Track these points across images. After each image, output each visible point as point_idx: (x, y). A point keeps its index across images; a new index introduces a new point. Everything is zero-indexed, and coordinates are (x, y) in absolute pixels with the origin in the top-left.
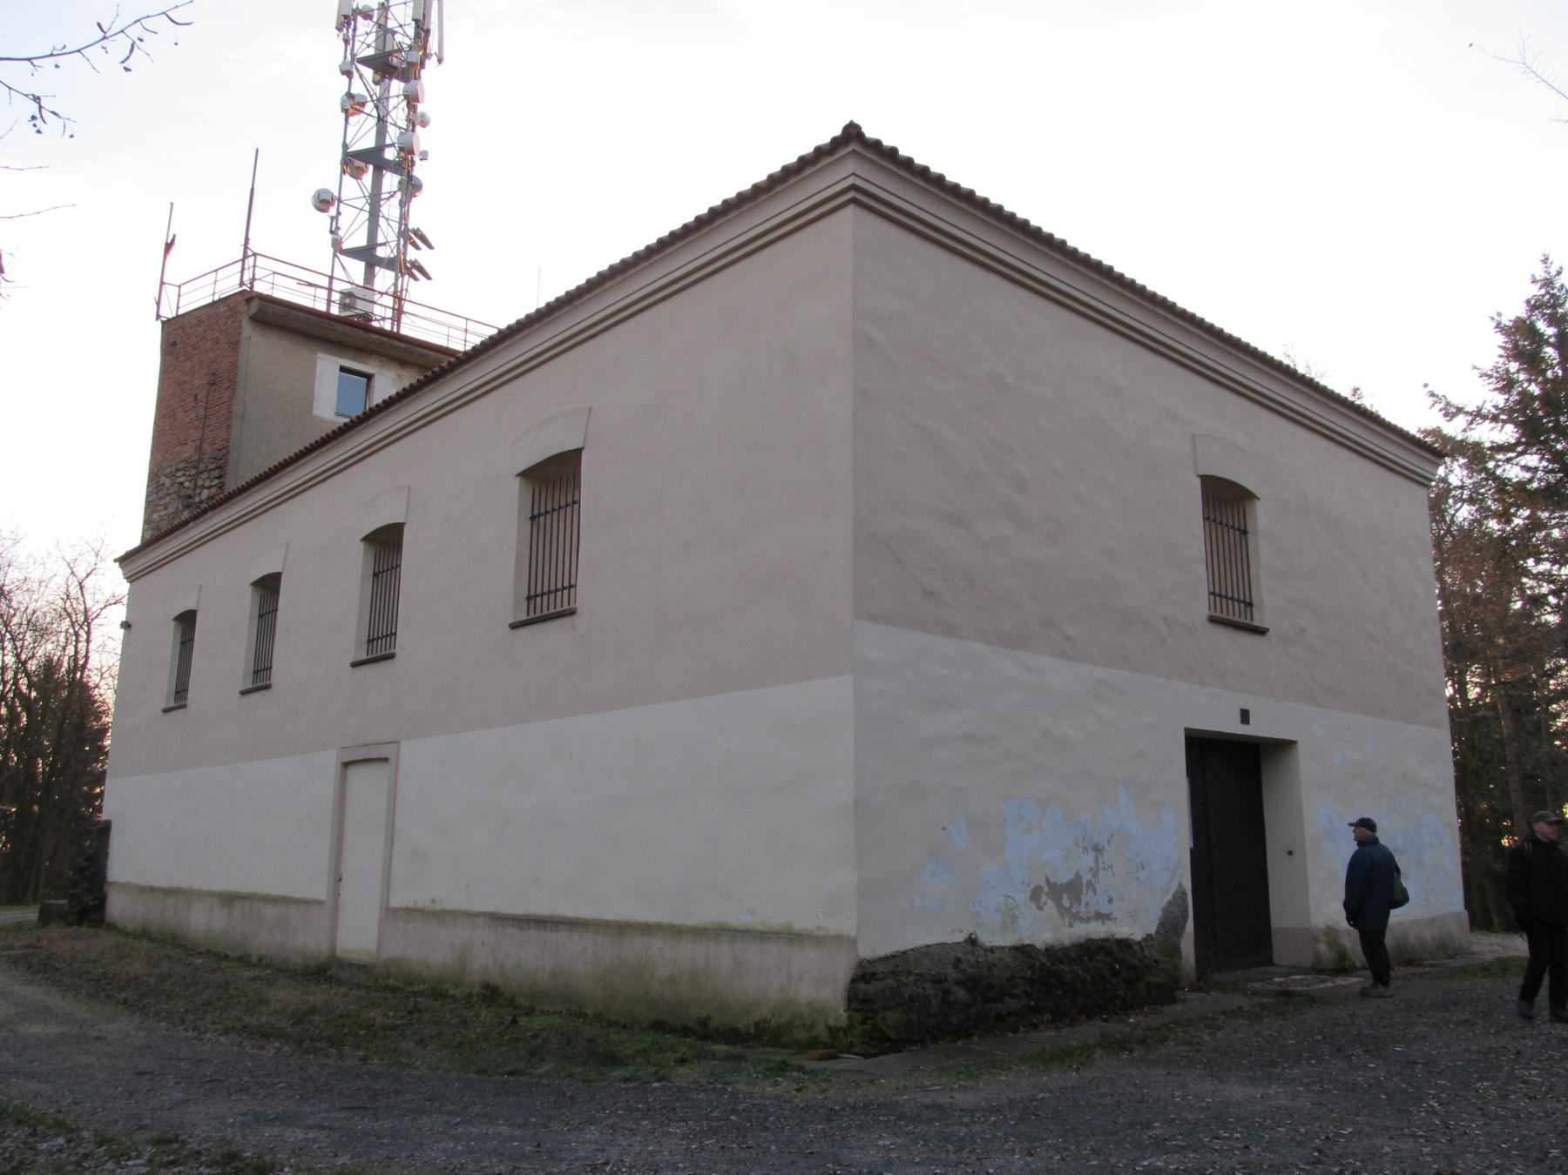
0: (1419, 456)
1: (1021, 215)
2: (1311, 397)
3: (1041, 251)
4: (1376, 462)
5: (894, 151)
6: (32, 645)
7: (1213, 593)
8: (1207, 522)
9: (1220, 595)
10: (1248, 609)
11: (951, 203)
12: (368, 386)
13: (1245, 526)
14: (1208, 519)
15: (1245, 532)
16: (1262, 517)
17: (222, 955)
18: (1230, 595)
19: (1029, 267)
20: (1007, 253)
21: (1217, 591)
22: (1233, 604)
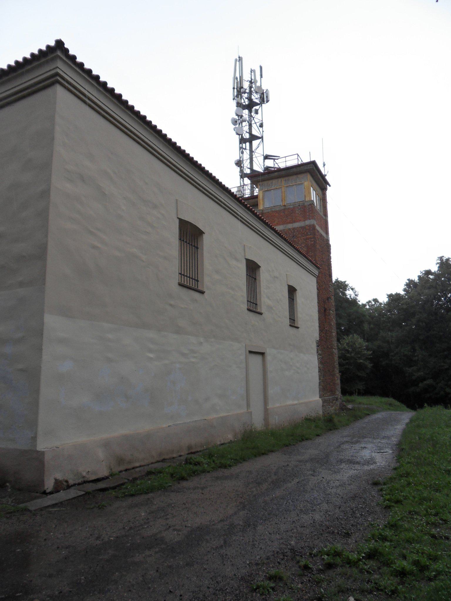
0: (285, 244)
1: (174, 140)
2: (306, 261)
3: (226, 195)
4: (267, 240)
5: (145, 117)
6: (239, 493)
7: (181, 274)
8: (247, 276)
9: (184, 275)
10: (196, 283)
11: (134, 119)
12: (264, 361)
13: (256, 277)
14: (248, 275)
15: (255, 279)
16: (207, 241)
17: (272, 581)
18: (250, 301)
19: (89, 93)
20: (78, 84)
21: (183, 273)
22: (192, 281)
